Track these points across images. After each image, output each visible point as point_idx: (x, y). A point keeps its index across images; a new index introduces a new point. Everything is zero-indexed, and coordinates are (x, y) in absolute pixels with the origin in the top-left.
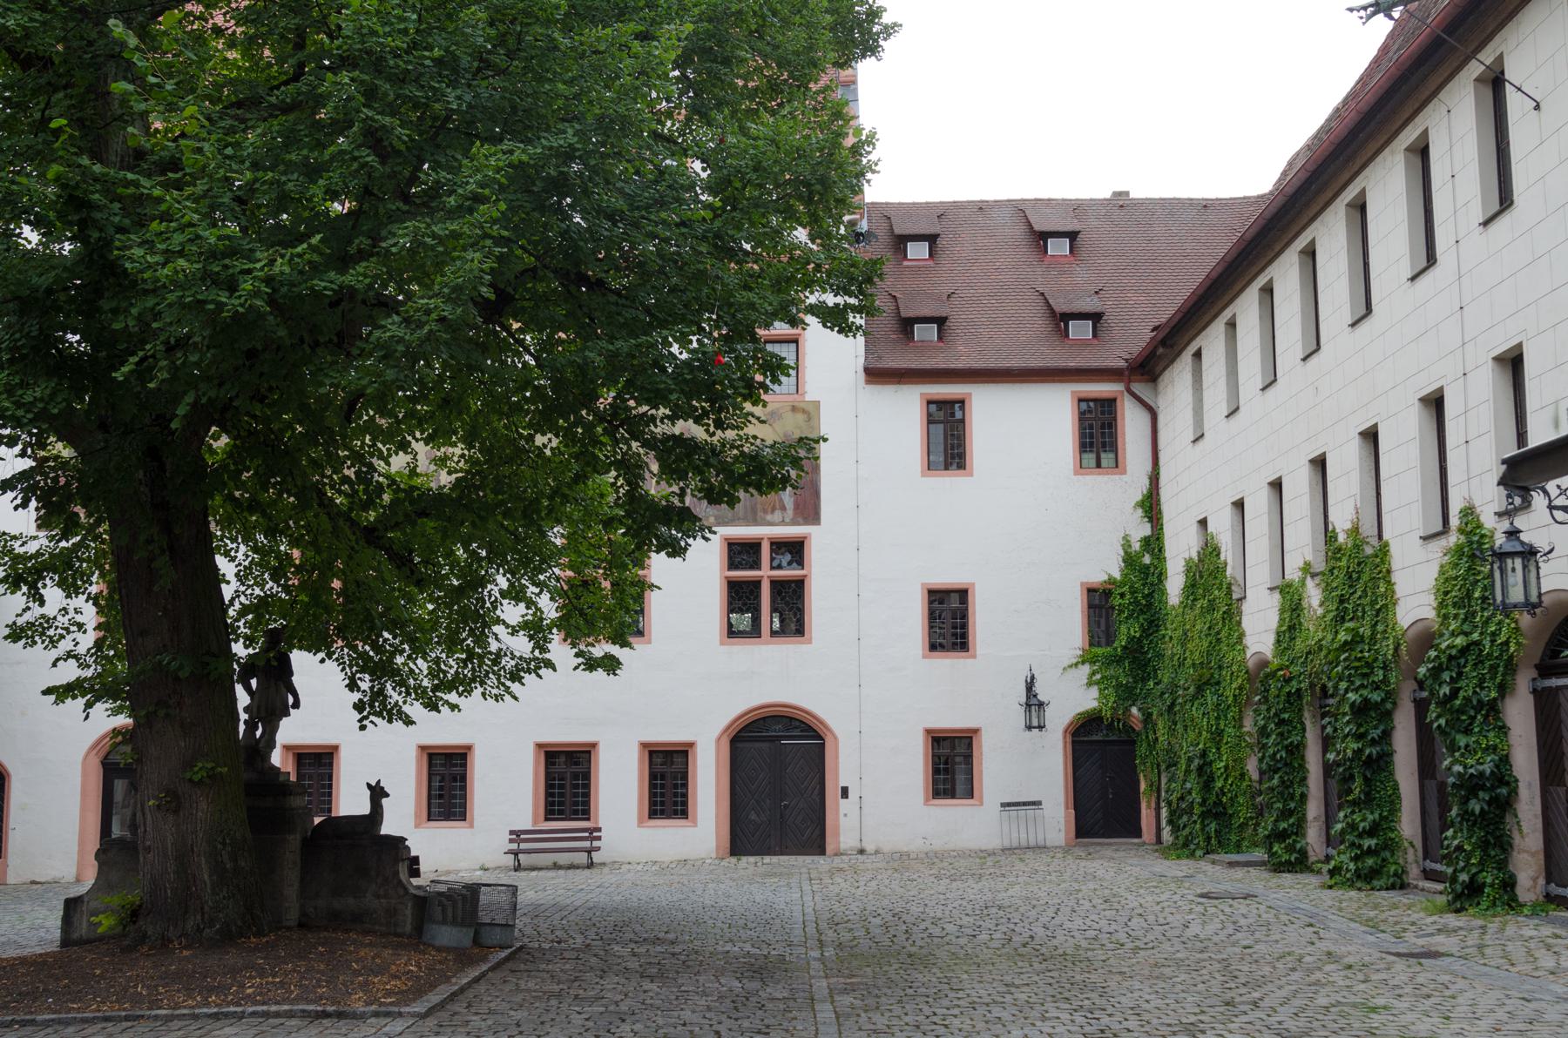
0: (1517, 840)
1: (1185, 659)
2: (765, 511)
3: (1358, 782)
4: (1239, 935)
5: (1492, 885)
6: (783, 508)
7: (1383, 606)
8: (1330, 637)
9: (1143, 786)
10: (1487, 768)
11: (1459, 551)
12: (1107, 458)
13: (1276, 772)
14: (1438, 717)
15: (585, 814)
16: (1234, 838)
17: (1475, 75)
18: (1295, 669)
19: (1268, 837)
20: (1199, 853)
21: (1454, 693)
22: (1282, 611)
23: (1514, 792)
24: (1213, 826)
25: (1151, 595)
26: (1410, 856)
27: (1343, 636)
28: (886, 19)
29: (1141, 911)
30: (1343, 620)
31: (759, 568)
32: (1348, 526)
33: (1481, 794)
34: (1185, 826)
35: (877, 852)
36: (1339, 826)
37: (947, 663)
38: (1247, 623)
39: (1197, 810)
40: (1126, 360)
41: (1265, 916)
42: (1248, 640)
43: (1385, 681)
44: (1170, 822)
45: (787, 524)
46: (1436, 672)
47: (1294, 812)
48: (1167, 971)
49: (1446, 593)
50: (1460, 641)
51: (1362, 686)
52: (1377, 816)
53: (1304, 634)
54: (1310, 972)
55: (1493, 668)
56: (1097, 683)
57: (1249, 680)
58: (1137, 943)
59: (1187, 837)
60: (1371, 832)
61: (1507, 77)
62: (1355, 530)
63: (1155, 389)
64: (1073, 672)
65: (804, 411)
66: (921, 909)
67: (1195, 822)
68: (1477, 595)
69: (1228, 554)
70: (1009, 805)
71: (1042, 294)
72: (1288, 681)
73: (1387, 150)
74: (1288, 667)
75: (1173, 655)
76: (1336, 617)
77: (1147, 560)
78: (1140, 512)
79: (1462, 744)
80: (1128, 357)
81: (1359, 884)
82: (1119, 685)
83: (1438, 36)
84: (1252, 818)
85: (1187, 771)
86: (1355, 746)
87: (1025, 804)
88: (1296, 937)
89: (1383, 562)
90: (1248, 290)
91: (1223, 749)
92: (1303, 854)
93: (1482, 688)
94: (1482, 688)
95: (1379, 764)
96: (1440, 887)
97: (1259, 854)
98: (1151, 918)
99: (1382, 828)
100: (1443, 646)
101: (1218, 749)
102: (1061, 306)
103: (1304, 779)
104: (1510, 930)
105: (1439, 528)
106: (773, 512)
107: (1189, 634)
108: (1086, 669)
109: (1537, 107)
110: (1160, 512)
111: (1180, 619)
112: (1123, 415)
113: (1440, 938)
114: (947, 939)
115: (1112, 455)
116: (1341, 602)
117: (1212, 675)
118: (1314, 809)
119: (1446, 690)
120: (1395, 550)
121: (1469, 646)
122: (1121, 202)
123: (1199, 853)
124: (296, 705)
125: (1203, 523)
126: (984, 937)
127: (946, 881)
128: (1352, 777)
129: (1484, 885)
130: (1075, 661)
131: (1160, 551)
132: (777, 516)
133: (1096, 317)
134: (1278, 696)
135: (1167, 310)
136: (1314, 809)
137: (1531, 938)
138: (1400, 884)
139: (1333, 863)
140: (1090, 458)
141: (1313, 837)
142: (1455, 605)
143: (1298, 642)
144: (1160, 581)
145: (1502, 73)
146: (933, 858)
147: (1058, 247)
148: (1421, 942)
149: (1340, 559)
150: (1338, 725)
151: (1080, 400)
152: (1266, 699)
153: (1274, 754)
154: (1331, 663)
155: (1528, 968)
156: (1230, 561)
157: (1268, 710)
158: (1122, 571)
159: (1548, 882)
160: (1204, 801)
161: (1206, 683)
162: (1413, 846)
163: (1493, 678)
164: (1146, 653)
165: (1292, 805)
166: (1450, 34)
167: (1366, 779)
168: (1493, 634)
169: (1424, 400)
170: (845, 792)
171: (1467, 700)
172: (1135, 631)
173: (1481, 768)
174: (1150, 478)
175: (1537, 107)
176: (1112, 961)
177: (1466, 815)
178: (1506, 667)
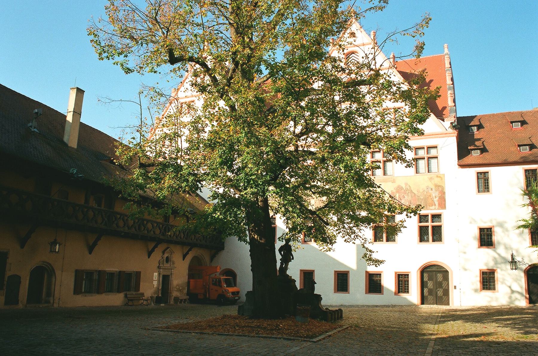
2: (430, 206)
6: (435, 205)
7: (273, 225)
15: (131, 274)
65: (440, 177)
124: (293, 259)
132: (433, 207)
170: (455, 287)
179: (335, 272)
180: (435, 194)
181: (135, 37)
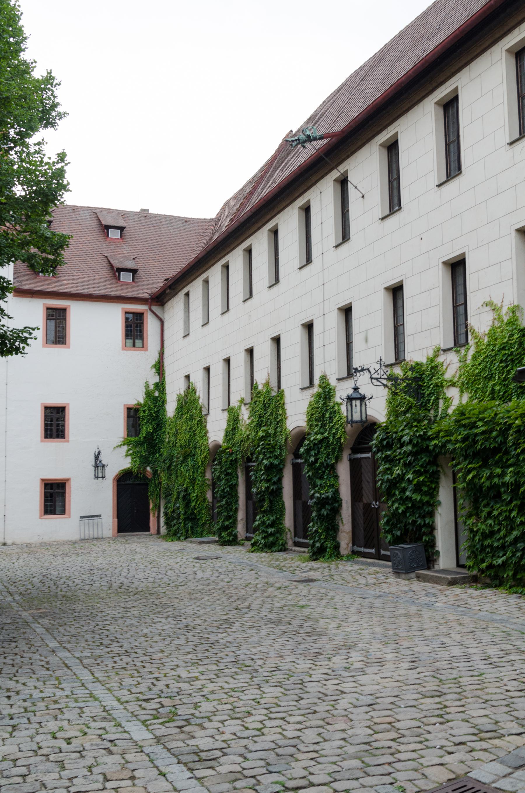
0: (341, 527)
1: (176, 443)
3: (267, 501)
4: (222, 577)
5: (330, 548)
8: (253, 434)
9: (151, 506)
10: (330, 494)
11: (319, 396)
12: (138, 342)
13: (224, 497)
14: (308, 472)
16: (199, 530)
17: (334, 178)
18: (235, 449)
19: (219, 529)
20: (182, 538)
21: (316, 460)
22: (229, 421)
23: (340, 505)
24: (190, 525)
25: (158, 411)
26: (289, 536)
27: (261, 434)
28: (59, 109)
29: (170, 567)
30: (260, 426)
32: (264, 381)
33: (327, 507)
34: (174, 525)
35: (13, 544)
36: (257, 523)
37: (54, 444)
38: (209, 427)
39: (182, 517)
40: (150, 294)
41: (230, 567)
42: (210, 435)
43: (280, 455)
44: (167, 523)
46: (308, 451)
47: (232, 517)
48: (197, 595)
49: (312, 415)
50: (319, 437)
51: (270, 457)
52: (274, 517)
53: (240, 432)
54: (263, 592)
55: (334, 449)
56: (131, 455)
57: (209, 454)
58: (176, 583)
59: (176, 530)
60: (272, 525)
61: (349, 179)
62: (267, 384)
63: (163, 309)
64: (119, 449)
66: (57, 572)
67: (181, 523)
68: (327, 416)
69: (201, 392)
70: (85, 517)
71: (106, 257)
72: (231, 454)
73: (290, 207)
74: (231, 448)
75: (169, 442)
76: (257, 424)
77: (157, 394)
78: (154, 370)
79: (319, 484)
80: (150, 293)
81: (266, 550)
82: (141, 456)
83: (321, 157)
84: (208, 520)
85: (178, 498)
86: (266, 485)
87: (92, 516)
88: (248, 576)
89: (281, 399)
90: (215, 266)
91: (196, 487)
92: (236, 536)
93: (329, 458)
94: (329, 458)
95: (277, 493)
96: (306, 550)
97: (216, 538)
98: (177, 571)
99: (277, 523)
100: (312, 439)
101: (193, 487)
102: (117, 264)
103: (237, 501)
104: (341, 567)
105: (308, 384)
107: (179, 431)
108: (125, 448)
109: (363, 197)
110: (163, 370)
111: (174, 423)
112: (147, 321)
113: (312, 573)
114: (78, 587)
115: (141, 341)
116: (260, 417)
117: (191, 451)
118: (241, 515)
119: (312, 459)
120: (287, 394)
121: (323, 439)
122: (144, 214)
123: (182, 538)
125: (188, 377)
126: (97, 585)
127: (59, 558)
128: (264, 500)
129: (327, 548)
130: (120, 444)
131: (163, 389)
133: (134, 271)
134: (226, 462)
135: (173, 272)
136: (241, 515)
137: (351, 571)
138: (284, 549)
139: (253, 540)
140: (130, 342)
141: (240, 528)
142: (316, 420)
143: (237, 436)
144: (163, 405)
145: (347, 177)
146: (46, 546)
147: (114, 234)
148: (304, 575)
149: (259, 397)
150: (258, 475)
151: (126, 313)
152: (220, 463)
153: (224, 489)
154: (254, 446)
155: (355, 584)
156: (201, 396)
157: (221, 468)
158: (144, 399)
159: (353, 545)
160: (185, 514)
161: (188, 455)
162: (290, 531)
163: (333, 454)
164: (155, 440)
165: (231, 513)
166: (327, 156)
167: (270, 501)
168: (334, 434)
169: (303, 325)
171: (322, 463)
172: (150, 429)
173: (327, 494)
174: (159, 353)
175: (363, 197)
176: (167, 592)
177: (319, 516)
178: (339, 449)
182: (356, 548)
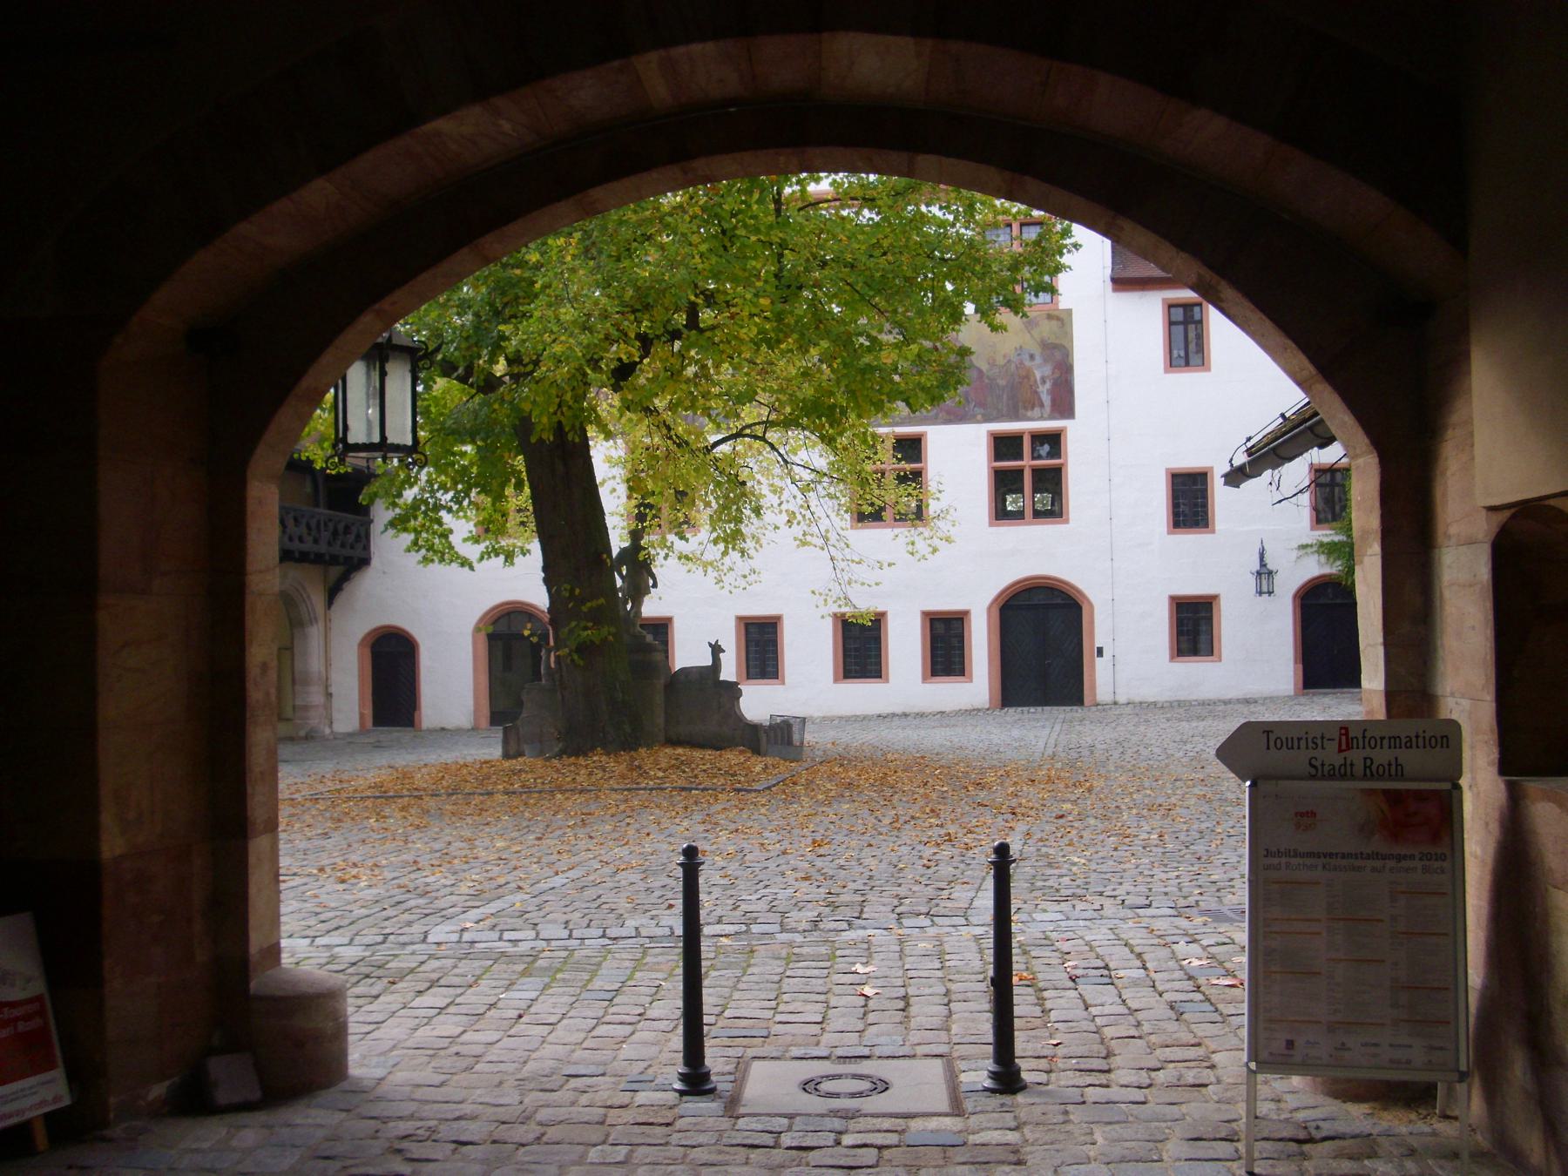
2: (1026, 408)
6: (1042, 405)
31: (1021, 458)
37: (1190, 540)
45: (1045, 419)
65: (1058, 318)
106: (1033, 408)
124: (655, 585)
132: (1037, 411)
179: (740, 619)
180: (1041, 371)
181: (1184, 723)
182: (1355, 746)
